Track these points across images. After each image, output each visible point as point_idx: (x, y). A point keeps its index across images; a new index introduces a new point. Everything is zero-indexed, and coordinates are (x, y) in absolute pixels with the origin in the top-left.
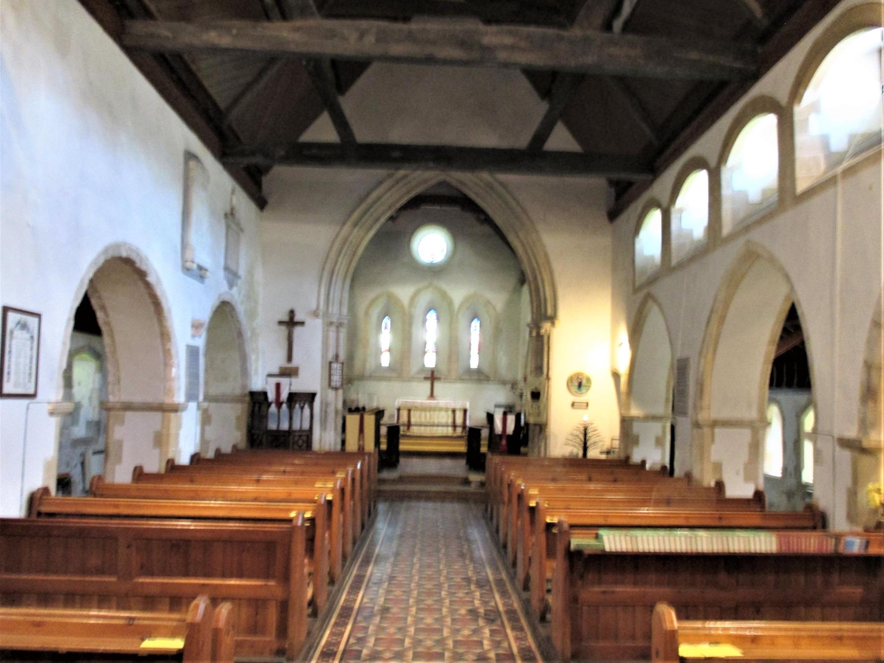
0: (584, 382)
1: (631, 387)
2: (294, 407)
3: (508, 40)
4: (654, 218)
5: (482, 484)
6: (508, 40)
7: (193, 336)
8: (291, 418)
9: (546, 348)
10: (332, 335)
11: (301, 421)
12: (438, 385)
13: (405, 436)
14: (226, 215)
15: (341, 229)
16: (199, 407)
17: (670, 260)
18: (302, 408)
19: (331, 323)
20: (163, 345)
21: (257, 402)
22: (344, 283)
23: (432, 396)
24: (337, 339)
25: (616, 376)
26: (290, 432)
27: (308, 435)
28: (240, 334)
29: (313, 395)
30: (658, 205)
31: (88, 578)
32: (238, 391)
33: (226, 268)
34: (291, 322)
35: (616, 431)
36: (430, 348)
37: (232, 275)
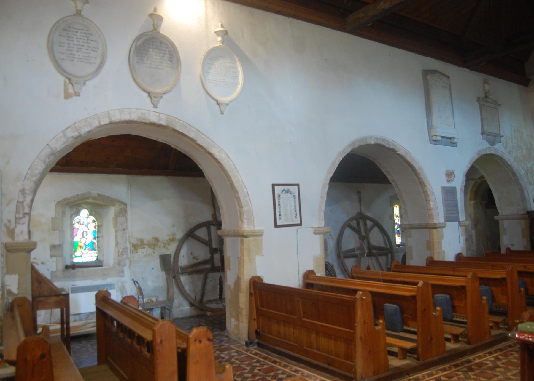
7: (448, 181)
14: (478, 100)
28: (514, 174)
31: (269, 310)
32: (522, 212)
37: (493, 137)
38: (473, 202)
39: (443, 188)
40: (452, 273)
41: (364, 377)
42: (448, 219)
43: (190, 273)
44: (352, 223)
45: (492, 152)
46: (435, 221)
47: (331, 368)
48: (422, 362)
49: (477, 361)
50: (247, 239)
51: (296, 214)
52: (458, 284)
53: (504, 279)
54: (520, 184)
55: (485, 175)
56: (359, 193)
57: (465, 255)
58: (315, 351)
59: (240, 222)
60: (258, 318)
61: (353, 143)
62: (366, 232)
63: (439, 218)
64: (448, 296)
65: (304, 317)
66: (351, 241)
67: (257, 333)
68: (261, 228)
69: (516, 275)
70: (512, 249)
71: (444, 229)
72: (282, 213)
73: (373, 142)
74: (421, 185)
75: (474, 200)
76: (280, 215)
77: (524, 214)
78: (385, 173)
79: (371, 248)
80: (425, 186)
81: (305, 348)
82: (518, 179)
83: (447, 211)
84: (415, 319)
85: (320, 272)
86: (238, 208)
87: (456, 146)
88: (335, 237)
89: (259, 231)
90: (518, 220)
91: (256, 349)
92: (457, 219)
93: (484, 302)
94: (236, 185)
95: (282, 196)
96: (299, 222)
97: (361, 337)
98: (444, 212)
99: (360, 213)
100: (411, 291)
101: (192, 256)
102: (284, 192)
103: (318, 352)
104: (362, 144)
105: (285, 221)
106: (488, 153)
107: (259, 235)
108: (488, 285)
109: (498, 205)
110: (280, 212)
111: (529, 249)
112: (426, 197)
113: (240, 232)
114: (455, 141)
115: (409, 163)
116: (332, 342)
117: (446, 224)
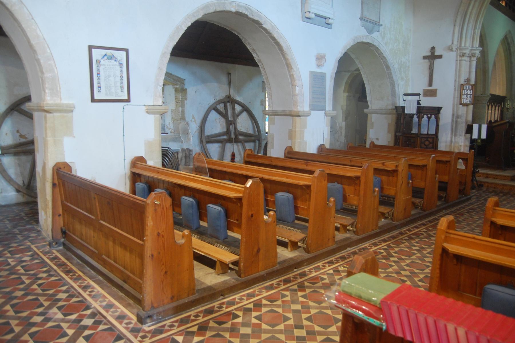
2: (423, 117)
7: (318, 66)
11: (426, 127)
18: (429, 118)
19: (463, 55)
20: (289, 72)
21: (400, 112)
28: (388, 67)
32: (390, 107)
34: (432, 57)
37: (372, 25)
38: (346, 94)
39: (311, 73)
41: (155, 305)
42: (313, 108)
43: (16, 154)
44: (218, 107)
45: (369, 41)
46: (300, 109)
47: (126, 286)
48: (243, 279)
49: (314, 274)
50: (51, 115)
51: (122, 88)
52: (302, 183)
53: (358, 178)
55: (360, 66)
56: (229, 74)
57: (328, 146)
58: (112, 262)
59: (43, 92)
60: (64, 214)
61: (207, 6)
62: (233, 117)
63: (304, 106)
64: (291, 196)
65: (101, 220)
66: (216, 125)
67: (64, 233)
68: (71, 102)
69: (371, 172)
70: (376, 143)
71: (308, 117)
72: (103, 85)
73: (233, 10)
74: (288, 67)
75: (348, 92)
76: (99, 87)
77: (392, 109)
78: (251, 51)
79: (238, 134)
80: (292, 69)
81: (104, 256)
82: (391, 73)
83: (313, 98)
84: (239, 226)
85: (154, 160)
86: (40, 74)
88: (199, 121)
89: (68, 105)
91: (58, 251)
92: (323, 108)
93: (331, 204)
94: (33, 42)
95: (102, 62)
96: (126, 98)
97: (152, 255)
98: (310, 99)
99: (229, 97)
100: (238, 191)
101: (19, 134)
102: (106, 57)
103: (115, 264)
104: (218, 9)
105: (106, 94)
106: (364, 41)
107: (69, 110)
108: (341, 184)
109: (369, 98)
110: (99, 83)
111: (392, 144)
112: (292, 81)
113: (42, 105)
114: (330, 21)
115: (276, 40)
116: (128, 254)
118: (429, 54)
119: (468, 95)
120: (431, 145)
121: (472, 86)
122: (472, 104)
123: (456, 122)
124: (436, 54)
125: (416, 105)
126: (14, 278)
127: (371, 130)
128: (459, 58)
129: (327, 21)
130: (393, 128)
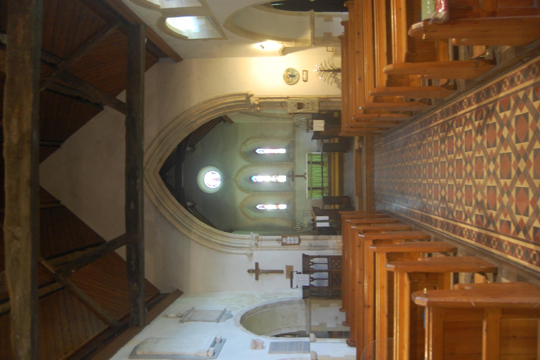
0: (290, 73)
1: (291, 39)
2: (313, 269)
3: (15, 122)
4: (173, 23)
5: (361, 139)
6: (15, 122)
7: (263, 348)
8: (320, 271)
9: (268, 100)
10: (264, 244)
11: (322, 264)
12: (297, 173)
13: (330, 193)
14: (182, 321)
15: (192, 240)
16: (314, 341)
17: (199, 7)
18: (313, 264)
19: (256, 245)
21: (310, 293)
22: (228, 237)
23: (304, 176)
24: (266, 240)
25: (285, 51)
26: (329, 271)
27: (330, 258)
28: (265, 307)
29: (304, 256)
30: (163, 20)
32: (304, 306)
33: (218, 321)
34: (257, 272)
35: (322, 50)
36: (273, 179)
37: (224, 316)
40: (371, 311)
54: (275, 303)
71: (318, 354)
77: (306, 304)
82: (271, 304)
83: (297, 350)
87: (225, 340)
90: (312, 312)
92: (308, 344)
100: (402, 282)
111: (340, 302)
117: (313, 352)
118: (254, 275)
119: (289, 240)
120: (339, 261)
121: (283, 237)
122: (298, 236)
123: (315, 247)
124: (254, 268)
125: (302, 275)
126: (501, 161)
127: (328, 326)
128: (259, 248)
129: (218, 342)
130: (325, 302)
